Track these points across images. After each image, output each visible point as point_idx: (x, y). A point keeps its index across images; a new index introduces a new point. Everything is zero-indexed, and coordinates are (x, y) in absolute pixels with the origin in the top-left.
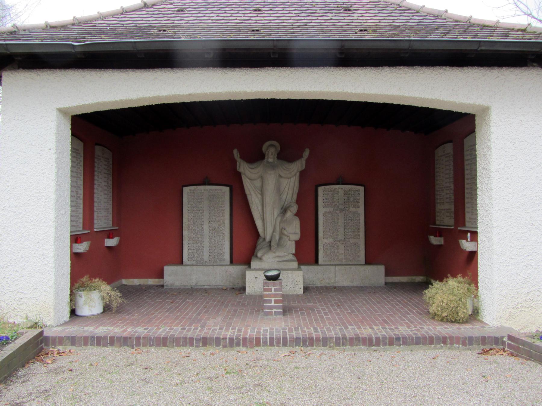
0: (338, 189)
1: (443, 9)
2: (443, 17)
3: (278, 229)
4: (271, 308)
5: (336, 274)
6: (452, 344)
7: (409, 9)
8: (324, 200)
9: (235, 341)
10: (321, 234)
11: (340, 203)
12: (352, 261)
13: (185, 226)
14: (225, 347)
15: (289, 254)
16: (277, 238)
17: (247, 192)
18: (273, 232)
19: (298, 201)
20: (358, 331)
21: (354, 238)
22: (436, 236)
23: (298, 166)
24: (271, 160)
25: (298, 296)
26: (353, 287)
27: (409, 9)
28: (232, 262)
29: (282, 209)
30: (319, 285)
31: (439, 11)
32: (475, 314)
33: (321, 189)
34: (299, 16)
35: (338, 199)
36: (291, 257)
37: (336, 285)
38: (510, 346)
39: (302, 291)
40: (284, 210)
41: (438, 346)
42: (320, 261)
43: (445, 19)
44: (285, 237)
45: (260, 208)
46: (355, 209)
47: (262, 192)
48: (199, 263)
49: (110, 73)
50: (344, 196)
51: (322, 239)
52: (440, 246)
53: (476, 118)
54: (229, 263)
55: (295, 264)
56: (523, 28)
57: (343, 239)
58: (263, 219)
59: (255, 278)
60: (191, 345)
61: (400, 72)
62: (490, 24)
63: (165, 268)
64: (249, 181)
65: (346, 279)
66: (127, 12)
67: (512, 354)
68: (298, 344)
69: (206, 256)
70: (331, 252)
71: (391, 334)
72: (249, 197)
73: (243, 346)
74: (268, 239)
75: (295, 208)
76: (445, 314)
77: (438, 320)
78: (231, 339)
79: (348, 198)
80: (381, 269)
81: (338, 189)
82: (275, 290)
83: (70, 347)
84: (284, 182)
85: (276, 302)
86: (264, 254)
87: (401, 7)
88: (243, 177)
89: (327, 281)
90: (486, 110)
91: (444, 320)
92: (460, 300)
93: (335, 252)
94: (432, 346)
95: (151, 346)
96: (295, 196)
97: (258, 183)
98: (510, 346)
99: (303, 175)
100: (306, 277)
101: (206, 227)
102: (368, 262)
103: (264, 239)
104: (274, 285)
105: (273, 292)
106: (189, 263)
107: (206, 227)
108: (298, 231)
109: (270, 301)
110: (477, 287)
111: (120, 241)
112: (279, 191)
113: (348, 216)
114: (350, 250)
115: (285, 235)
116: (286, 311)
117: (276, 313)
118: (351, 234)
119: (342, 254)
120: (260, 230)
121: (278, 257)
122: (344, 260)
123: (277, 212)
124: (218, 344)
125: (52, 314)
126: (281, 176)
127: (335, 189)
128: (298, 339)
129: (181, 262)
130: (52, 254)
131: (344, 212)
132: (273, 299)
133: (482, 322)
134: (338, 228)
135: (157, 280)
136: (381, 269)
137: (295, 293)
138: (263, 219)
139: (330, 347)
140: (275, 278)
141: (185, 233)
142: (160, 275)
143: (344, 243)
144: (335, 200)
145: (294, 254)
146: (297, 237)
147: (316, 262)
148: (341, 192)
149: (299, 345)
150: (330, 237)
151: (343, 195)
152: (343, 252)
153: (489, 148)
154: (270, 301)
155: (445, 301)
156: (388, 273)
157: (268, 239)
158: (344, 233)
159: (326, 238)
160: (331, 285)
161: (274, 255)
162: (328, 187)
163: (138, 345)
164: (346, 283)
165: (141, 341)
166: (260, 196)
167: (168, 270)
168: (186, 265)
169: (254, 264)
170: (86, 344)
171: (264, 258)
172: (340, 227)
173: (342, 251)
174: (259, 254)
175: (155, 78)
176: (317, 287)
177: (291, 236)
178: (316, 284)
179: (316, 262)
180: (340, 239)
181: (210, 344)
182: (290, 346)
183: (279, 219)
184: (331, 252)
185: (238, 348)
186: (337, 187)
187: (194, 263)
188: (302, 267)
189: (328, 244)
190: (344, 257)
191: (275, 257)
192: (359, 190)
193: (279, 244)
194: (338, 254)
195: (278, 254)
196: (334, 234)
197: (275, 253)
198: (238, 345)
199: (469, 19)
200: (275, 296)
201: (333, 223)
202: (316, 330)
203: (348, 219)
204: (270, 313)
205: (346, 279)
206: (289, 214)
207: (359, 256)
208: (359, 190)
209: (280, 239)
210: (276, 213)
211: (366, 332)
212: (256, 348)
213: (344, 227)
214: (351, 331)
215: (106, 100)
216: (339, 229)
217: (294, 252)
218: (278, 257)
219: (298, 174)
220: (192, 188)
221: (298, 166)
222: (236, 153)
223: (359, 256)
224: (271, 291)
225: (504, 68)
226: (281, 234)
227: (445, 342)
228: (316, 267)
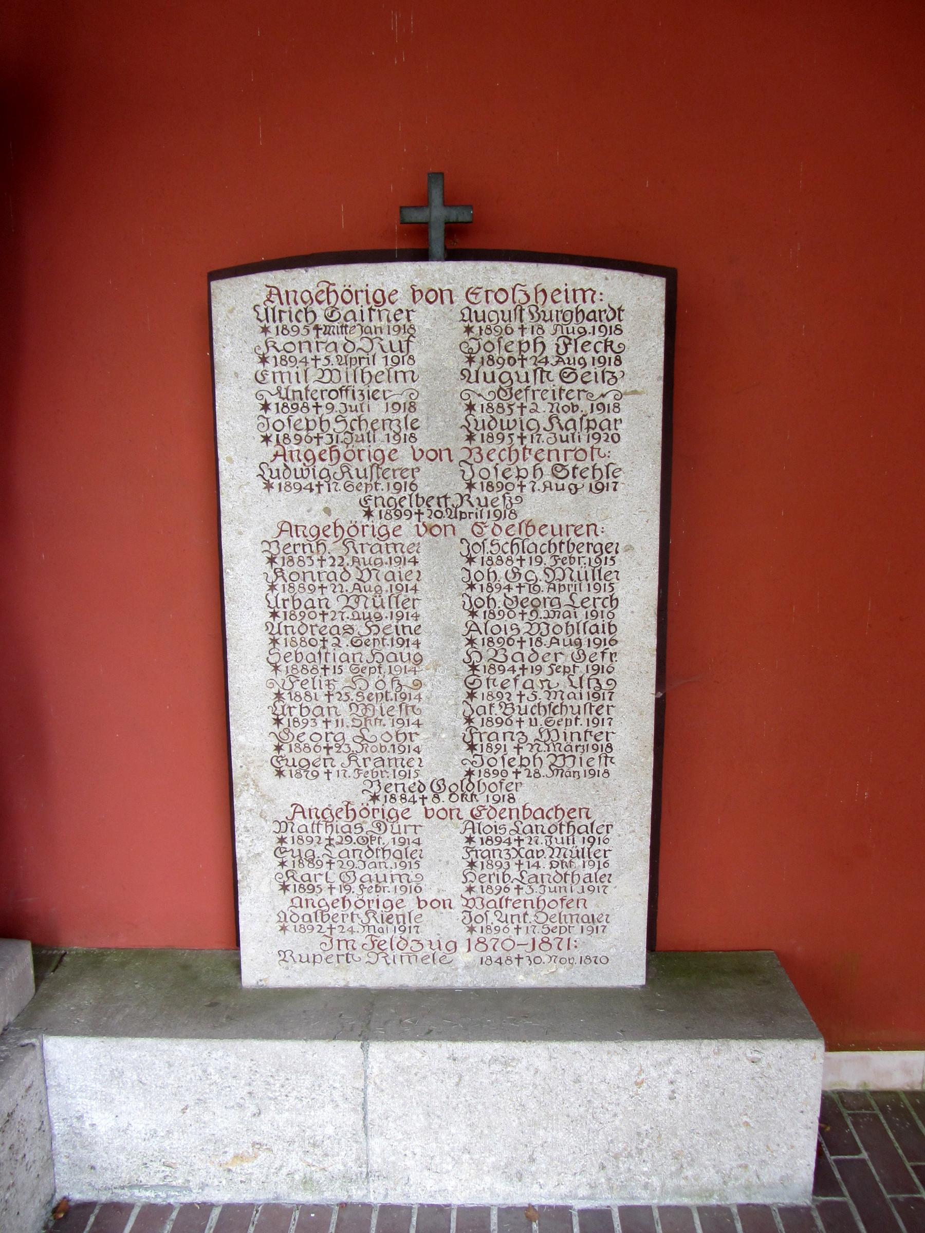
0: (403, 301)
5: (376, 1109)
8: (272, 414)
11: (424, 441)
12: (533, 961)
21: (557, 771)
35: (412, 406)
46: (566, 496)
50: (464, 375)
51: (267, 776)
57: (454, 775)
59: (235, 373)
65: (466, 1150)
70: (346, 887)
79: (506, 391)
81: (403, 301)
89: (295, 1162)
93: (378, 889)
100: (101, 1129)
113: (501, 570)
114: (514, 872)
118: (532, 733)
119: (446, 904)
122: (463, 957)
127: (380, 300)
131: (464, 527)
134: (407, 679)
143: (466, 808)
144: (377, 411)
150: (341, 759)
151: (457, 362)
152: (454, 888)
158: (462, 726)
159: (305, 769)
172: (423, 674)
178: (194, 1183)
180: (426, 778)
184: (346, 887)
189: (323, 816)
190: (460, 933)
192: (618, 312)
194: (410, 902)
196: (375, 731)
201: (360, 628)
203: (499, 597)
205: (466, 1150)
207: (595, 924)
208: (618, 312)
213: (465, 670)
216: (418, 684)
223: (595, 924)
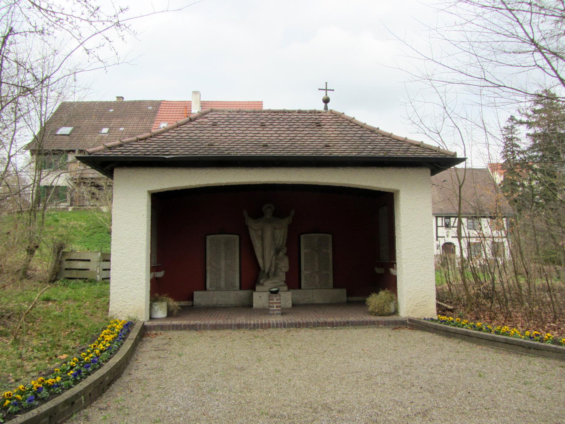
1: (376, 127)
2: (376, 132)
3: (274, 265)
4: (274, 310)
6: (378, 325)
7: (357, 125)
9: (256, 326)
10: (303, 268)
13: (208, 263)
14: (250, 329)
15: (281, 281)
16: (273, 270)
17: (252, 239)
18: (270, 266)
19: (287, 245)
20: (326, 320)
22: (379, 267)
23: (286, 222)
24: (268, 217)
25: (288, 308)
26: (326, 304)
27: (357, 125)
28: (241, 288)
29: (276, 250)
30: (302, 303)
31: (374, 128)
32: (396, 312)
33: (302, 237)
34: (289, 130)
36: (283, 283)
37: (314, 302)
38: (410, 325)
39: (290, 306)
40: (277, 252)
41: (370, 326)
42: (302, 287)
43: (377, 134)
44: (278, 270)
45: (261, 250)
47: (262, 239)
48: (218, 289)
49: (518, 356)
52: (382, 274)
53: (394, 195)
54: (239, 289)
55: (286, 288)
56: (418, 144)
58: (263, 258)
60: (231, 328)
61: (348, 170)
62: (401, 140)
63: (195, 292)
64: (253, 231)
66: (180, 125)
67: (410, 329)
68: (292, 327)
69: (223, 284)
71: (345, 320)
72: (254, 242)
73: (261, 329)
74: (266, 272)
75: (285, 250)
76: (377, 311)
77: (373, 315)
78: (254, 324)
80: (344, 291)
82: (276, 300)
83: (160, 331)
84: (277, 232)
85: (277, 307)
86: (264, 281)
87: (351, 122)
88: (249, 229)
90: (398, 191)
91: (376, 314)
92: (385, 302)
94: (367, 326)
95: (208, 329)
96: (285, 242)
97: (259, 233)
98: (410, 325)
99: (290, 228)
101: (223, 263)
102: (335, 286)
103: (264, 271)
104: (276, 297)
105: (275, 301)
106: (210, 289)
107: (223, 263)
108: (287, 265)
109: (273, 307)
110: (397, 296)
111: (165, 274)
112: (274, 238)
115: (278, 268)
116: (282, 314)
117: (277, 314)
120: (261, 265)
121: (274, 283)
123: (273, 253)
124: (246, 328)
125: (144, 315)
126: (275, 228)
128: (292, 323)
129: (205, 289)
130: (144, 278)
132: (275, 305)
133: (399, 316)
135: (187, 302)
136: (344, 291)
137: (286, 307)
138: (263, 258)
139: (310, 328)
140: (276, 292)
141: (208, 268)
142: (191, 298)
145: (284, 281)
146: (286, 269)
147: (300, 287)
148: (306, 272)
149: (293, 327)
152: (318, 280)
153: (400, 214)
154: (273, 307)
155: (377, 303)
156: (349, 294)
157: (266, 272)
160: (310, 302)
161: (271, 282)
162: (307, 235)
163: (200, 329)
164: (320, 301)
165: (202, 327)
166: (261, 242)
167: (197, 294)
168: (208, 291)
169: (258, 288)
170: (169, 330)
171: (265, 284)
173: (317, 280)
174: (261, 281)
175: (207, 173)
176: (300, 304)
177: (283, 269)
179: (300, 287)
181: (242, 328)
182: (288, 328)
183: (274, 258)
185: (258, 330)
186: (313, 235)
187: (214, 289)
188: (290, 290)
191: (272, 283)
193: (275, 275)
195: (274, 281)
197: (272, 280)
198: (258, 328)
199: (390, 135)
200: (276, 303)
202: (302, 320)
204: (273, 314)
206: (281, 254)
209: (275, 271)
210: (272, 254)
211: (330, 320)
212: (268, 329)
214: (322, 320)
215: (177, 186)
217: (284, 280)
218: (274, 283)
219: (287, 226)
220: (213, 236)
221: (286, 222)
222: (245, 213)
224: (274, 300)
225: (407, 168)
226: (276, 267)
227: (374, 324)
228: (300, 290)
